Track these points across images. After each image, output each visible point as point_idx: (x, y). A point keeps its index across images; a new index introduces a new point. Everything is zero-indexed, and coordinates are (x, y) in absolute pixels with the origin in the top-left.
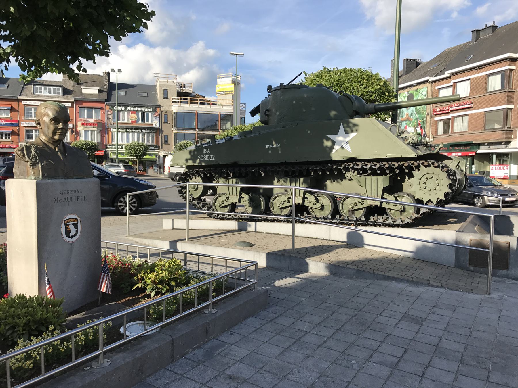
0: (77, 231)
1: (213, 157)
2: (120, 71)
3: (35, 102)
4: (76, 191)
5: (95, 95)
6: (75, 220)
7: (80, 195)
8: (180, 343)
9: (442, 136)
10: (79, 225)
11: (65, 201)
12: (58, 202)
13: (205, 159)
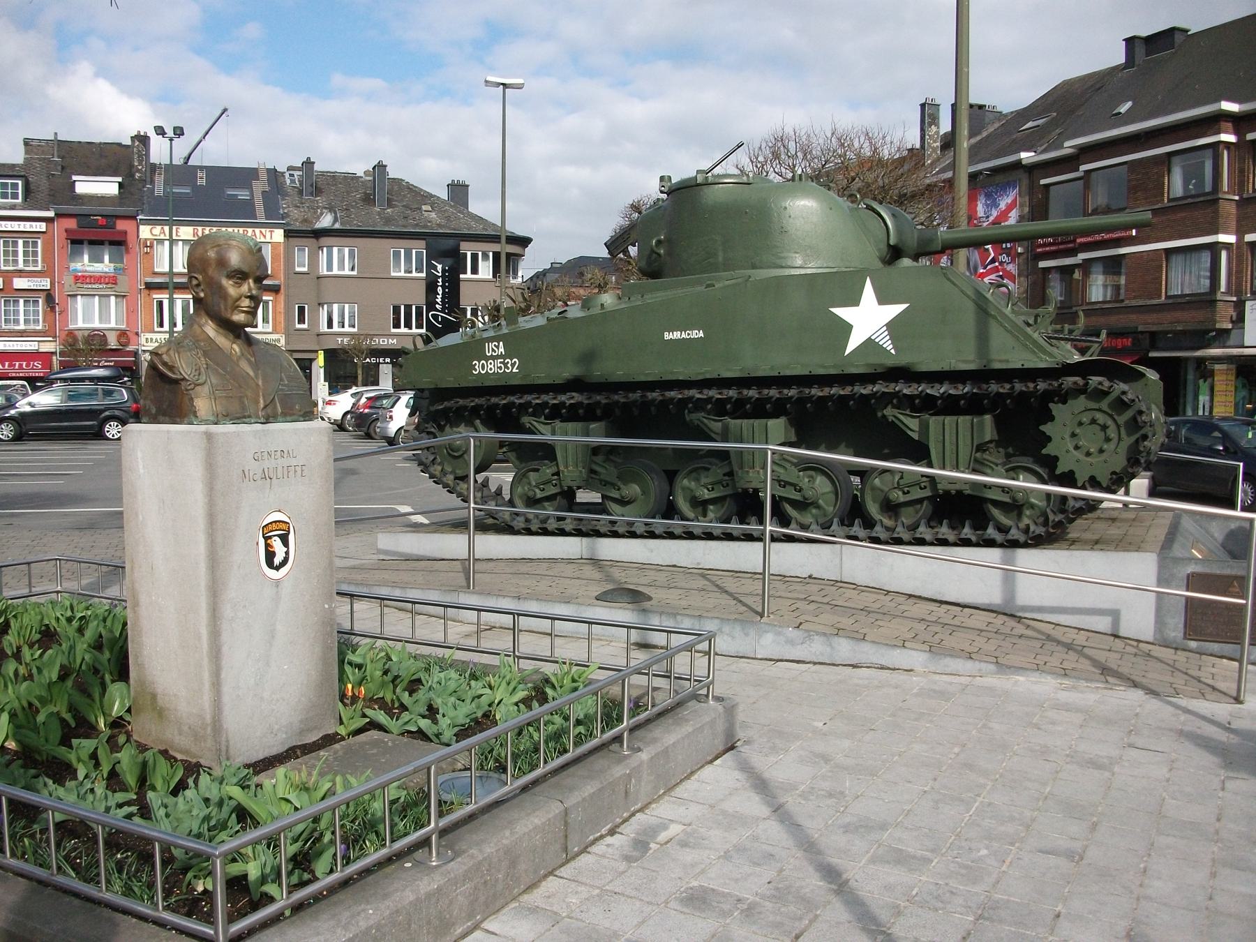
0: (287, 553)
1: (513, 365)
2: (179, 132)
3: (34, 224)
6: (284, 526)
7: (294, 462)
10: (291, 538)
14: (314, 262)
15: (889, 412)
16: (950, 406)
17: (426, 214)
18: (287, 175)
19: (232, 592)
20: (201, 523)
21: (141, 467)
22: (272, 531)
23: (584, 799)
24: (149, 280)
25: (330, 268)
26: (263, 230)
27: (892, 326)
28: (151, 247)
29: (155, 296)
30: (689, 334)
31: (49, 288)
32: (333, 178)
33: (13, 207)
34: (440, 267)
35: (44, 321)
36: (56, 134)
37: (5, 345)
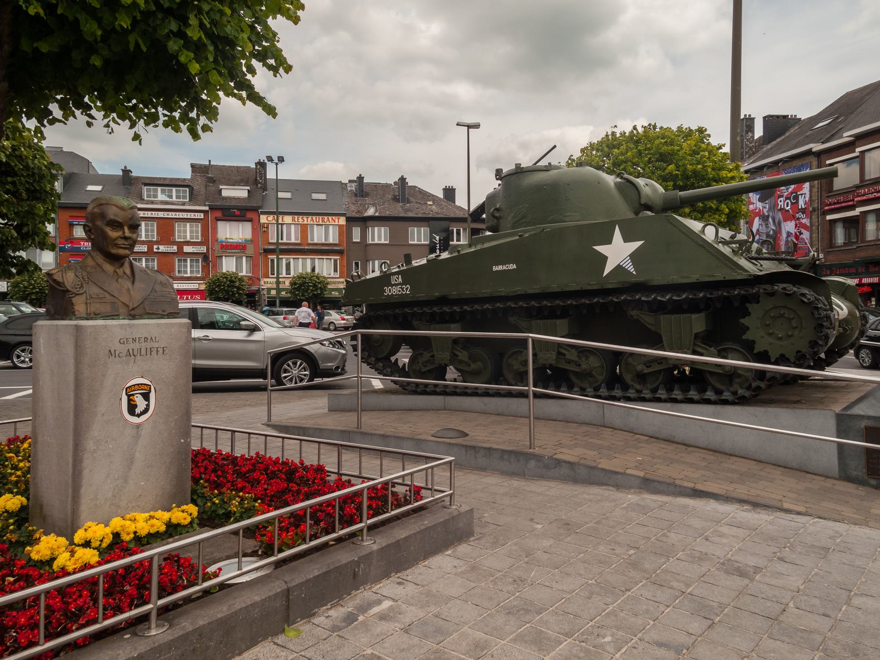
0: (148, 405)
1: (407, 289)
2: (281, 159)
4: (149, 338)
5: (244, 199)
6: (146, 387)
7: (156, 345)
8: (303, 596)
9: (842, 248)
10: (152, 396)
11: (129, 354)
12: (115, 357)
13: (394, 292)
14: (364, 235)
15: (634, 313)
16: (677, 308)
17: (430, 207)
18: (348, 185)
19: (96, 431)
20: (72, 387)
21: (42, 349)
22: (134, 391)
23: (308, 581)
24: (266, 247)
25: (373, 239)
26: (334, 217)
27: (633, 256)
28: (267, 228)
29: (269, 257)
30: (507, 267)
31: (205, 251)
32: (376, 186)
33: (184, 204)
34: (437, 238)
35: (202, 272)
36: (210, 161)
37: (178, 286)
